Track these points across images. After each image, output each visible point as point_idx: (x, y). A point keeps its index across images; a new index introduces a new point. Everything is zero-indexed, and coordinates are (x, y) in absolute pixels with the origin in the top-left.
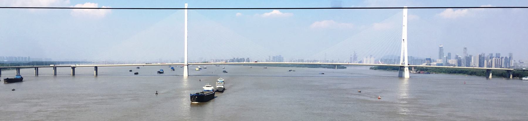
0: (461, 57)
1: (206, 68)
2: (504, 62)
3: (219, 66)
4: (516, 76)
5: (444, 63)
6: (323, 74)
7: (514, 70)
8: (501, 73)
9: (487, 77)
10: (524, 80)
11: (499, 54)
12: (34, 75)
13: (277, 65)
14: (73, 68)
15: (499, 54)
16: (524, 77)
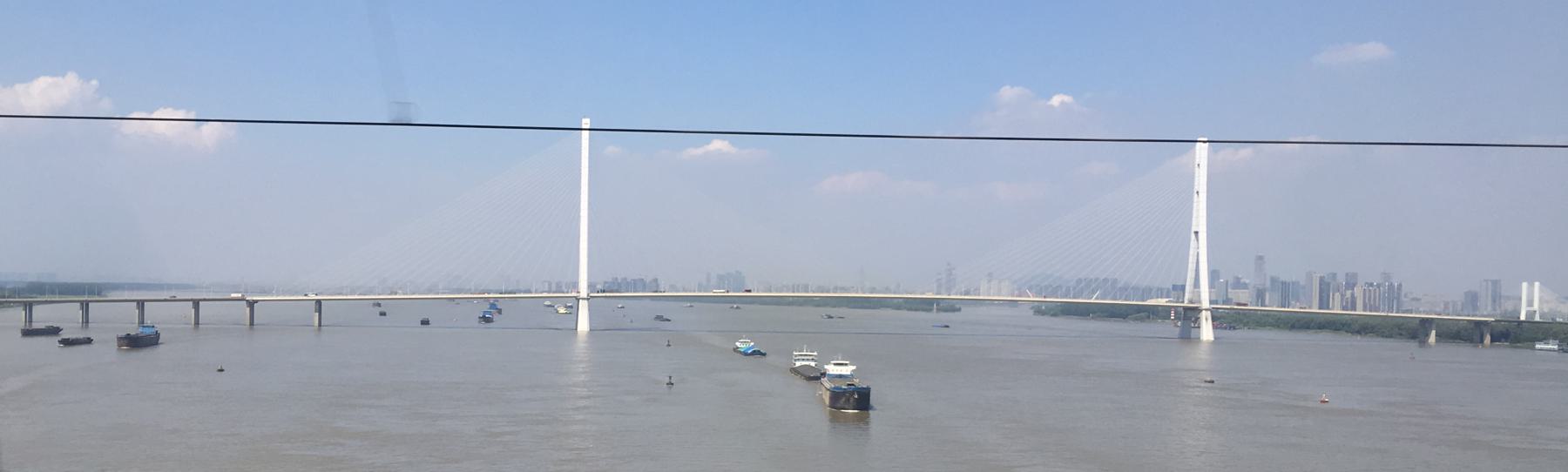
0: (1247, 281)
4: (1503, 340)
5: (1220, 300)
6: (947, 327)
7: (1496, 321)
9: (1420, 342)
10: (1541, 350)
12: (191, 324)
13: (745, 299)
14: (141, 304)
16: (1539, 341)
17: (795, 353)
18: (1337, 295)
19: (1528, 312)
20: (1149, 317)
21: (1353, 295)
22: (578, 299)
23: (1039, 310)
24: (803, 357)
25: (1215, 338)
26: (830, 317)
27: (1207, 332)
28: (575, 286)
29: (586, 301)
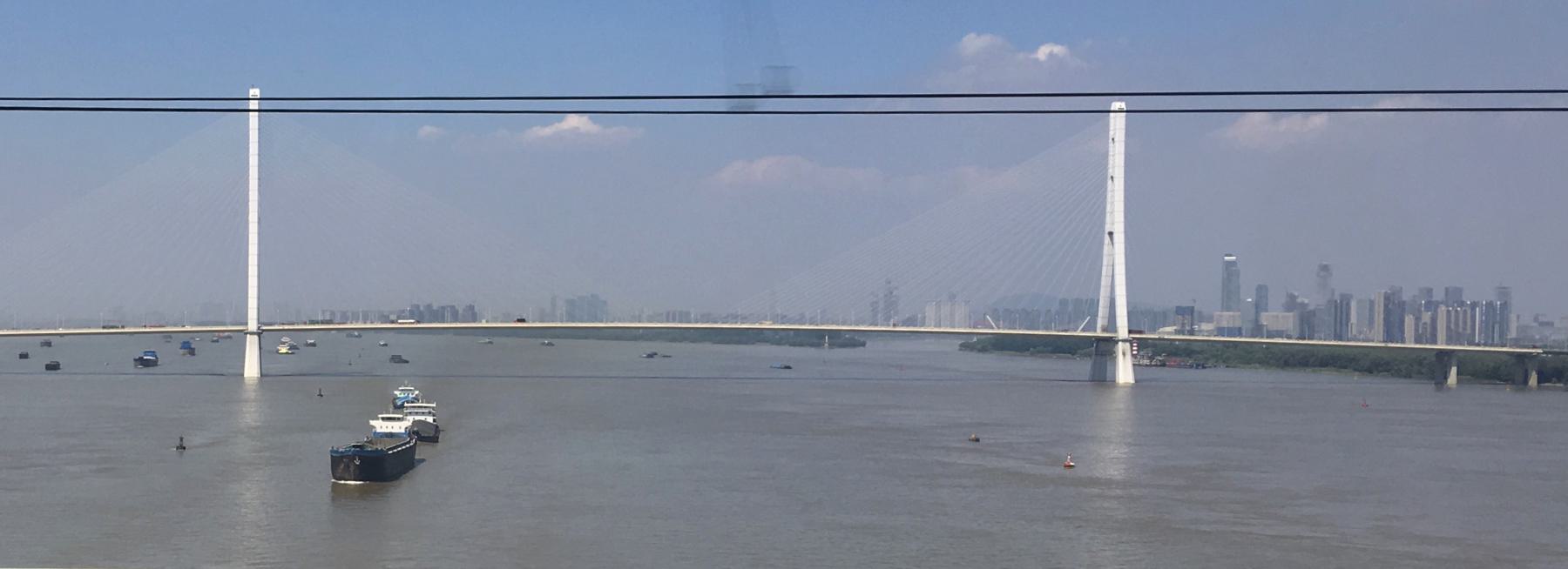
0: (1306, 301)
1: (313, 345)
2: (1481, 321)
3: (359, 336)
6: (789, 368)
8: (1492, 364)
11: (1459, 291)
15: (1459, 291)
23: (971, 345)
25: (1136, 381)
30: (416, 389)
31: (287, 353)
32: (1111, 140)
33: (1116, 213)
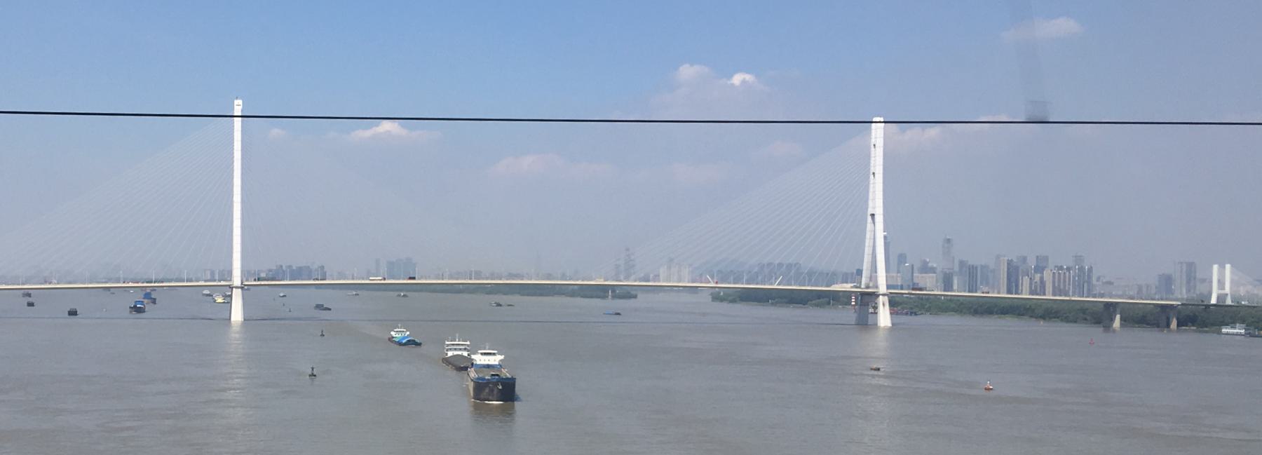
0: (935, 265)
4: (1190, 324)
6: (619, 314)
7: (1182, 304)
10: (1227, 334)
17: (447, 343)
18: (1026, 280)
19: (1218, 298)
20: (829, 303)
21: (1042, 279)
22: (231, 288)
23: (718, 297)
24: (455, 347)
25: (893, 324)
26: (499, 305)
27: (884, 317)
28: (228, 274)
29: (240, 290)
30: (407, 331)
31: (224, 302)
32: (872, 146)
33: (877, 200)
